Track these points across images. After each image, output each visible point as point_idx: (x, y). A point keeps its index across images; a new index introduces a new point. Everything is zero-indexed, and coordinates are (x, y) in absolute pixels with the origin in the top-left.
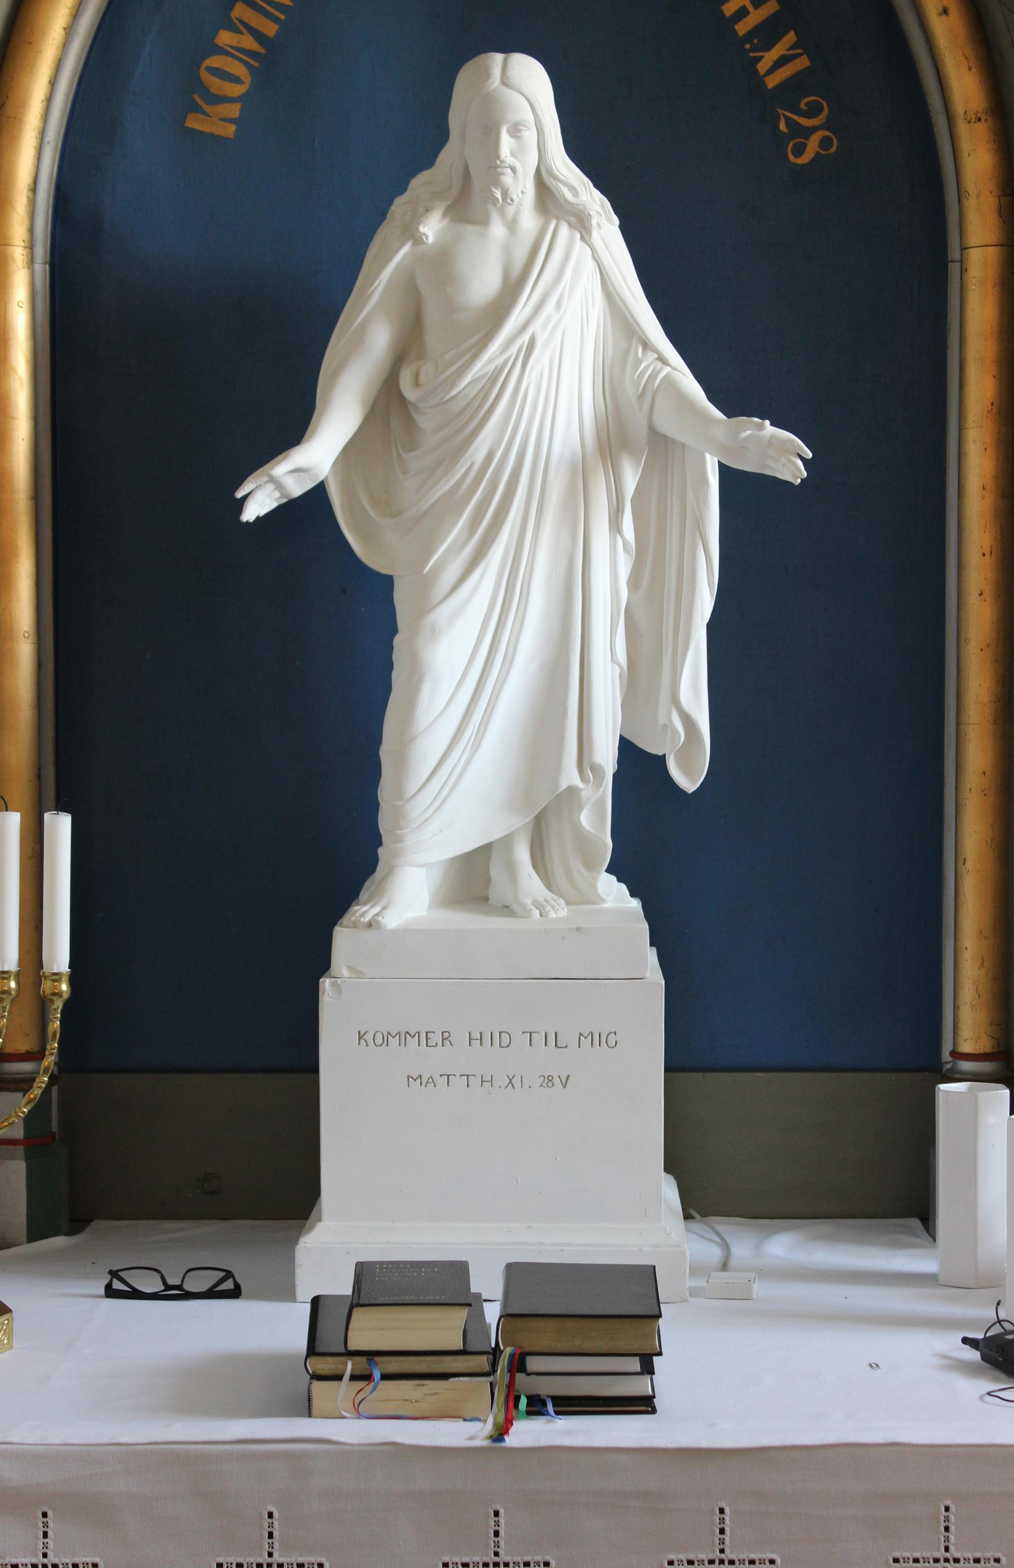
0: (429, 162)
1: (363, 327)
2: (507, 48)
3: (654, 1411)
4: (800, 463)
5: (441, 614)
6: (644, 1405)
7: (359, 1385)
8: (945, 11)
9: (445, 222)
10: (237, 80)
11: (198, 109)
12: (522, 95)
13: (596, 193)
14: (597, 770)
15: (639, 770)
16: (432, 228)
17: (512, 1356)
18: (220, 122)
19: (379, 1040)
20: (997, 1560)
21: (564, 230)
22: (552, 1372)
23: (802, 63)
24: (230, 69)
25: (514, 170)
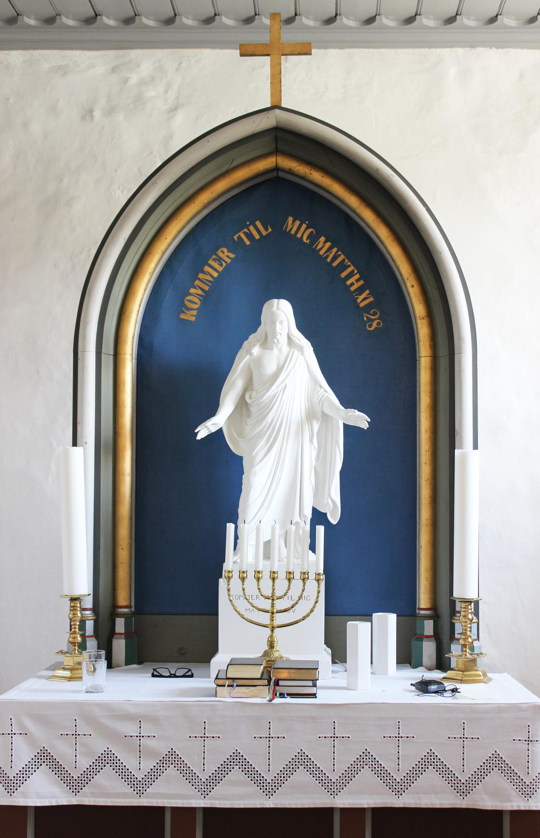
0: (255, 331)
1: (234, 381)
2: (279, 297)
3: (316, 697)
4: (367, 423)
5: (257, 468)
6: (314, 695)
7: (230, 688)
8: (413, 286)
9: (260, 349)
10: (196, 303)
11: (184, 312)
12: (281, 313)
13: (306, 340)
14: (305, 516)
15: (318, 517)
16: (256, 351)
17: (275, 680)
18: (190, 316)
19: (237, 598)
20: (413, 737)
21: (296, 351)
22: (285, 687)
23: (371, 299)
24: (194, 300)
25: (280, 334)
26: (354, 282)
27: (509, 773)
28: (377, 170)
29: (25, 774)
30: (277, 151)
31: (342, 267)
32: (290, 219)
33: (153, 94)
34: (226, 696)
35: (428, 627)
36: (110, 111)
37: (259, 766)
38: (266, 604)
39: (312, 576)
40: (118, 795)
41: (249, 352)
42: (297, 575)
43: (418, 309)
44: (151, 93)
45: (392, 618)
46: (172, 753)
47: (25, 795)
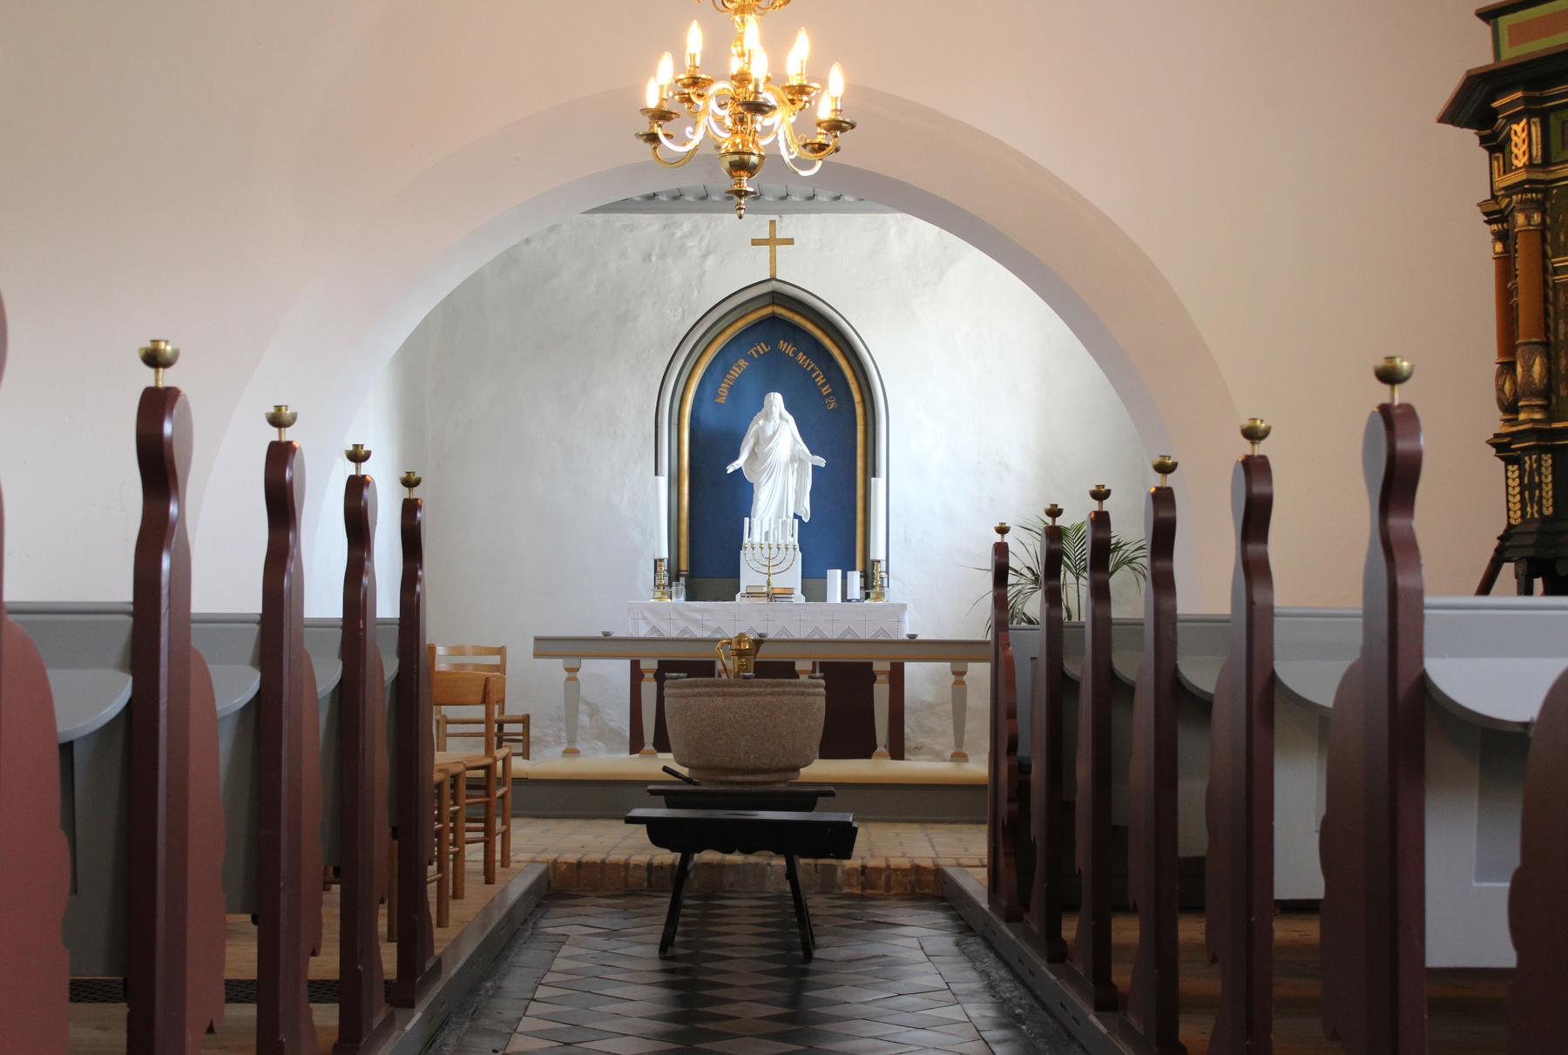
12: (776, 400)
18: (722, 400)
26: (820, 380)
30: (773, 304)
31: (813, 370)
34: (746, 601)
36: (662, 256)
43: (857, 397)
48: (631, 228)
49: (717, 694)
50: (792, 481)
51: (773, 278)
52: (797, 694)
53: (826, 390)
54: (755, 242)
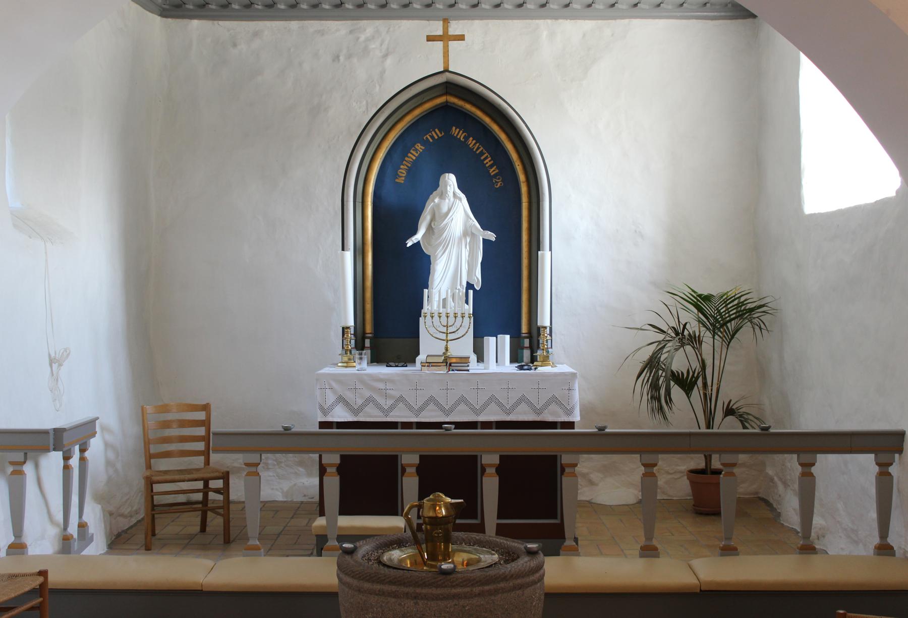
2: (449, 172)
12: (451, 180)
15: (470, 286)
16: (437, 200)
18: (401, 180)
24: (403, 171)
26: (488, 162)
27: (559, 403)
28: (500, 105)
29: (332, 407)
30: (446, 94)
31: (482, 153)
32: (454, 128)
33: (373, 46)
34: (426, 370)
35: (527, 342)
36: (349, 56)
37: (442, 402)
38: (444, 330)
39: (467, 315)
40: (376, 417)
41: (433, 201)
42: (459, 315)
43: (522, 177)
44: (372, 46)
45: (508, 337)
46: (401, 397)
47: (333, 417)
48: (322, 33)
49: (407, 595)
50: (465, 254)
51: (446, 70)
52: (514, 588)
53: (493, 171)
54: (430, 39)
